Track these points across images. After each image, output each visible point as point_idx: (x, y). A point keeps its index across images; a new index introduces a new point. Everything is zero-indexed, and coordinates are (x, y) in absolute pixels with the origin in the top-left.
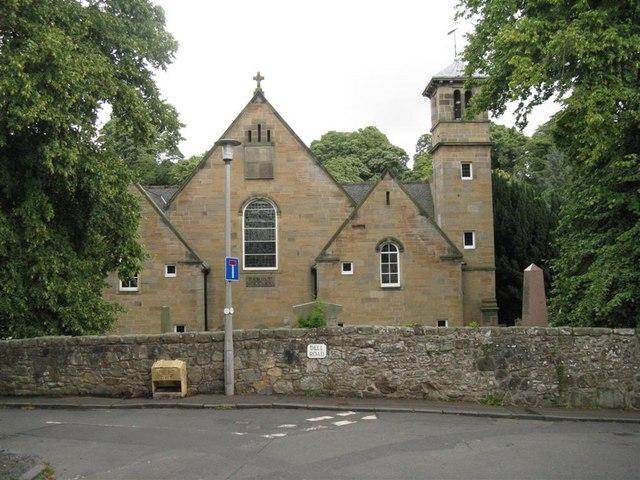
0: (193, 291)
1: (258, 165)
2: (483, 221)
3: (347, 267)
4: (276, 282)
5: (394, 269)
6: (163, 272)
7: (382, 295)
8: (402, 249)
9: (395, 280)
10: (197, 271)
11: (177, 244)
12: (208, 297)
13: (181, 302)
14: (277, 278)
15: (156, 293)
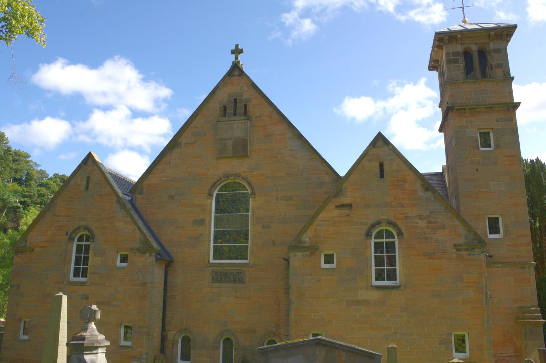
1: (230, 143)
6: (114, 261)
7: (374, 295)
9: (392, 276)
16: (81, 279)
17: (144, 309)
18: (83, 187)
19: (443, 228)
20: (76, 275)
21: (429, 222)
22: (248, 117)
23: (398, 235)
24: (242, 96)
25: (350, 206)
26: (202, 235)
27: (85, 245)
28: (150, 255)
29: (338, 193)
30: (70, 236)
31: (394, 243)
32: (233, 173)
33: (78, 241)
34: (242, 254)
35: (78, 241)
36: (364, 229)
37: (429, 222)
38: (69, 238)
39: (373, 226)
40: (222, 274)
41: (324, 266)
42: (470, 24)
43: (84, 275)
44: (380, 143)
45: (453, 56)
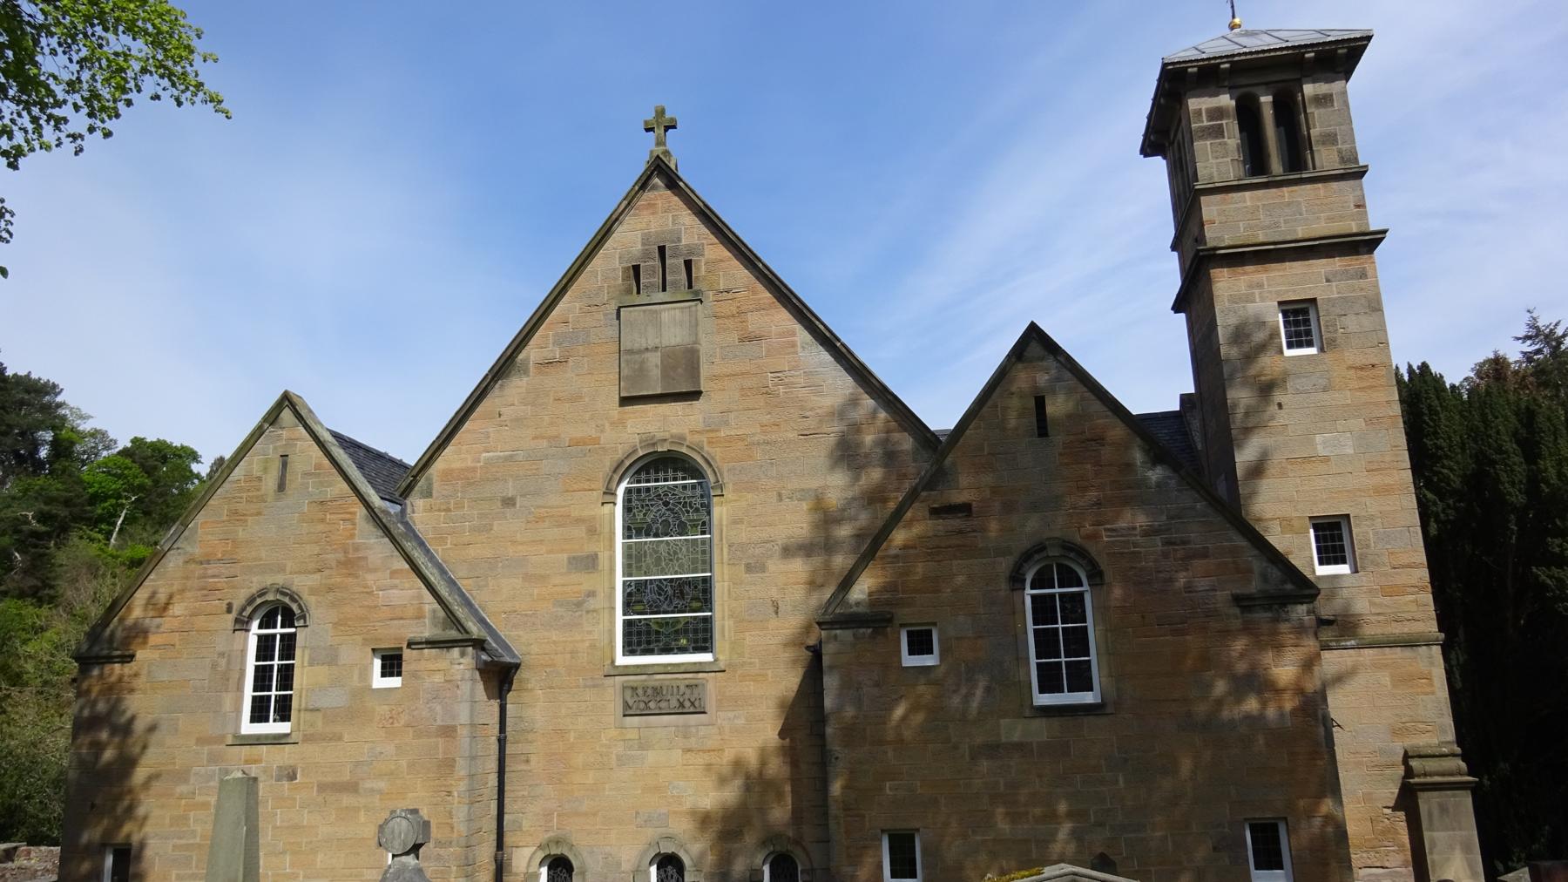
0: (448, 731)
1: (654, 360)
2: (1377, 479)
3: (920, 644)
4: (710, 703)
5: (1078, 641)
6: (366, 673)
7: (1039, 731)
8: (1096, 576)
9: (1081, 680)
10: (461, 664)
11: (409, 592)
12: (509, 749)
13: (411, 765)
14: (712, 683)
15: (340, 738)
16: (273, 727)
17: (449, 793)
18: (271, 481)
19: (1204, 554)
20: (259, 714)
21: (1168, 543)
22: (697, 293)
23: (1089, 577)
24: (679, 240)
25: (965, 509)
26: (592, 594)
27: (282, 635)
28: (463, 655)
29: (936, 478)
30: (240, 613)
31: (1081, 594)
32: (667, 435)
33: (260, 627)
34: (701, 638)
35: (260, 627)
36: (1004, 565)
37: (1168, 543)
38: (237, 621)
39: (1027, 557)
40: (649, 692)
41: (909, 661)
42: (1248, 34)
43: (284, 713)
44: (1035, 349)
45: (1211, 118)
